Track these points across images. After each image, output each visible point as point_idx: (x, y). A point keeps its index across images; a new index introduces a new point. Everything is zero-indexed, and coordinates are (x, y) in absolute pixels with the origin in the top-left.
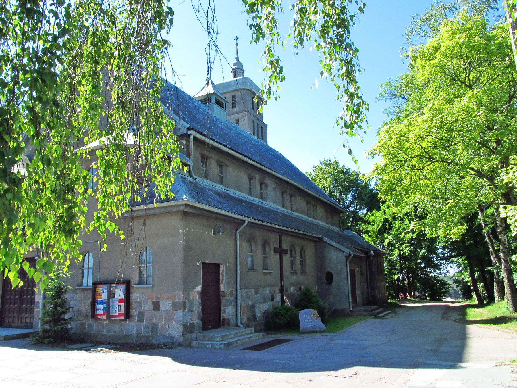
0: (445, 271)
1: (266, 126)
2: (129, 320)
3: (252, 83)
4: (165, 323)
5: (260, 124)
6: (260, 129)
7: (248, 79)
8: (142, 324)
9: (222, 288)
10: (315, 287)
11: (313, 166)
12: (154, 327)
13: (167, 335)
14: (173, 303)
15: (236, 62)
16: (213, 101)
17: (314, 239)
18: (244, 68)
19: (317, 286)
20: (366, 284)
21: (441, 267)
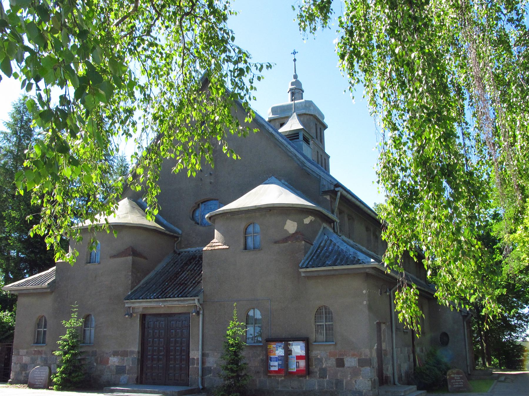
0: (524, 335)
1: (328, 157)
2: (309, 377)
3: (316, 109)
4: (351, 379)
5: (320, 153)
7: (310, 104)
8: (325, 379)
11: (375, 204)
12: (339, 383)
13: (355, 390)
14: (358, 359)
15: (295, 80)
16: (301, 137)
18: (303, 88)
21: (518, 329)
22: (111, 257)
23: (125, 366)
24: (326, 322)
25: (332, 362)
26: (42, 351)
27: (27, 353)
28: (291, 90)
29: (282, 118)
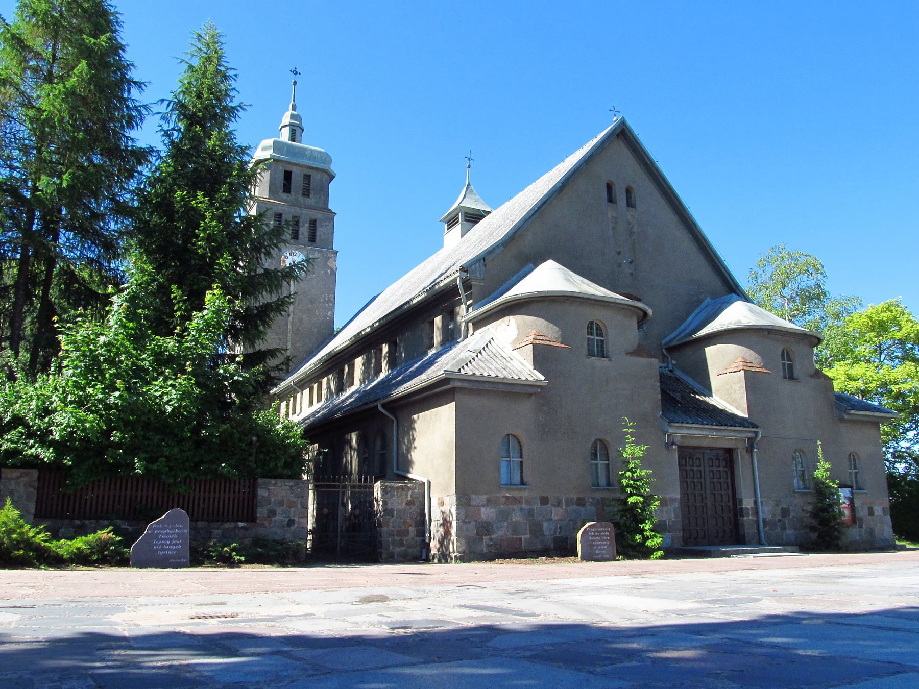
12: (871, 532)
22: (627, 354)
23: (665, 521)
24: (597, 464)
25: (866, 511)
26: (521, 497)
27: (488, 500)
28: (290, 125)
29: (289, 163)
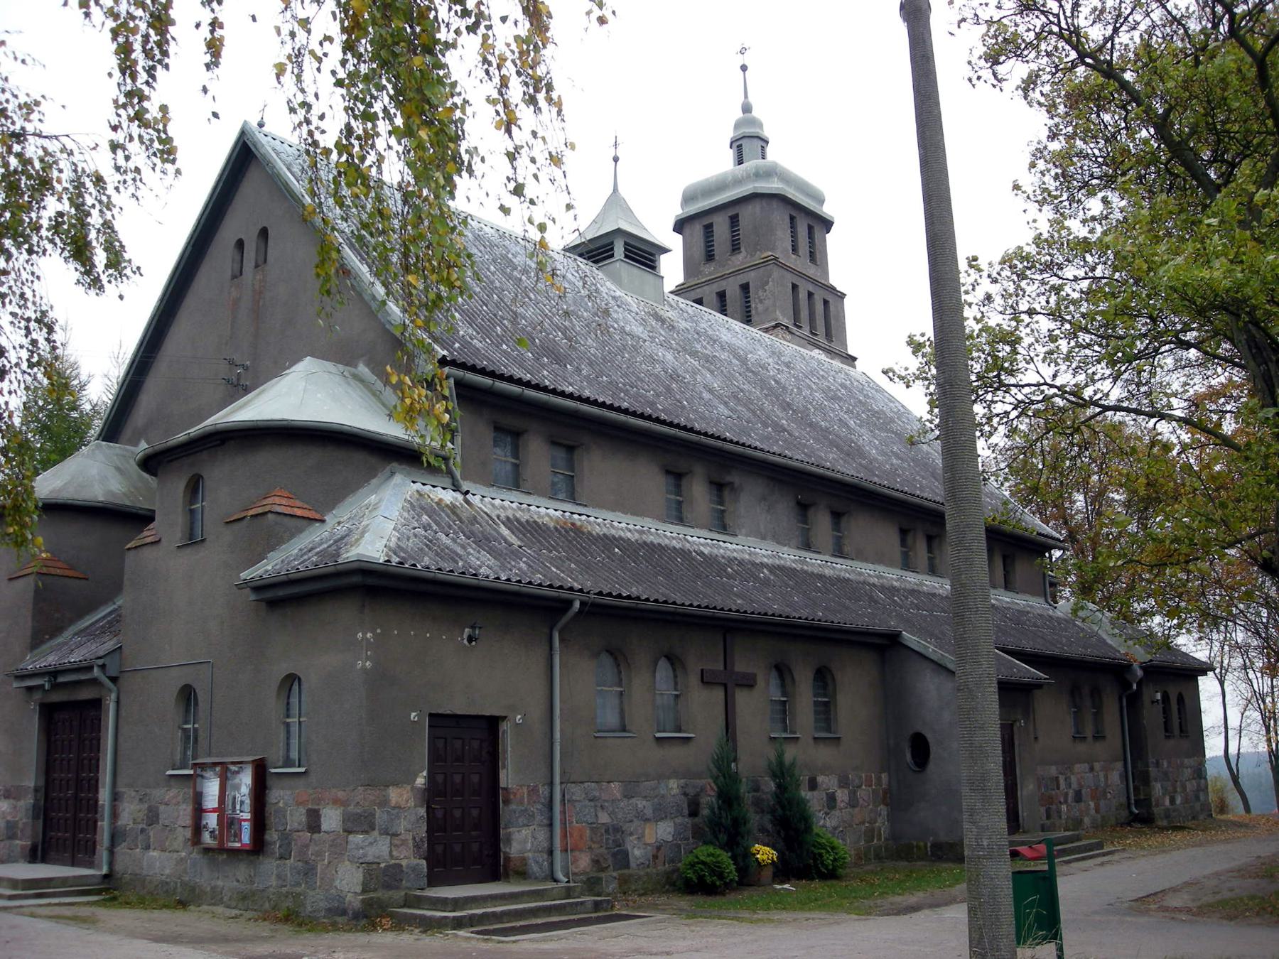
6: (819, 307)
9: (507, 778)
10: (879, 779)
16: (619, 251)
17: (877, 641)
19: (884, 776)
20: (1119, 765)
